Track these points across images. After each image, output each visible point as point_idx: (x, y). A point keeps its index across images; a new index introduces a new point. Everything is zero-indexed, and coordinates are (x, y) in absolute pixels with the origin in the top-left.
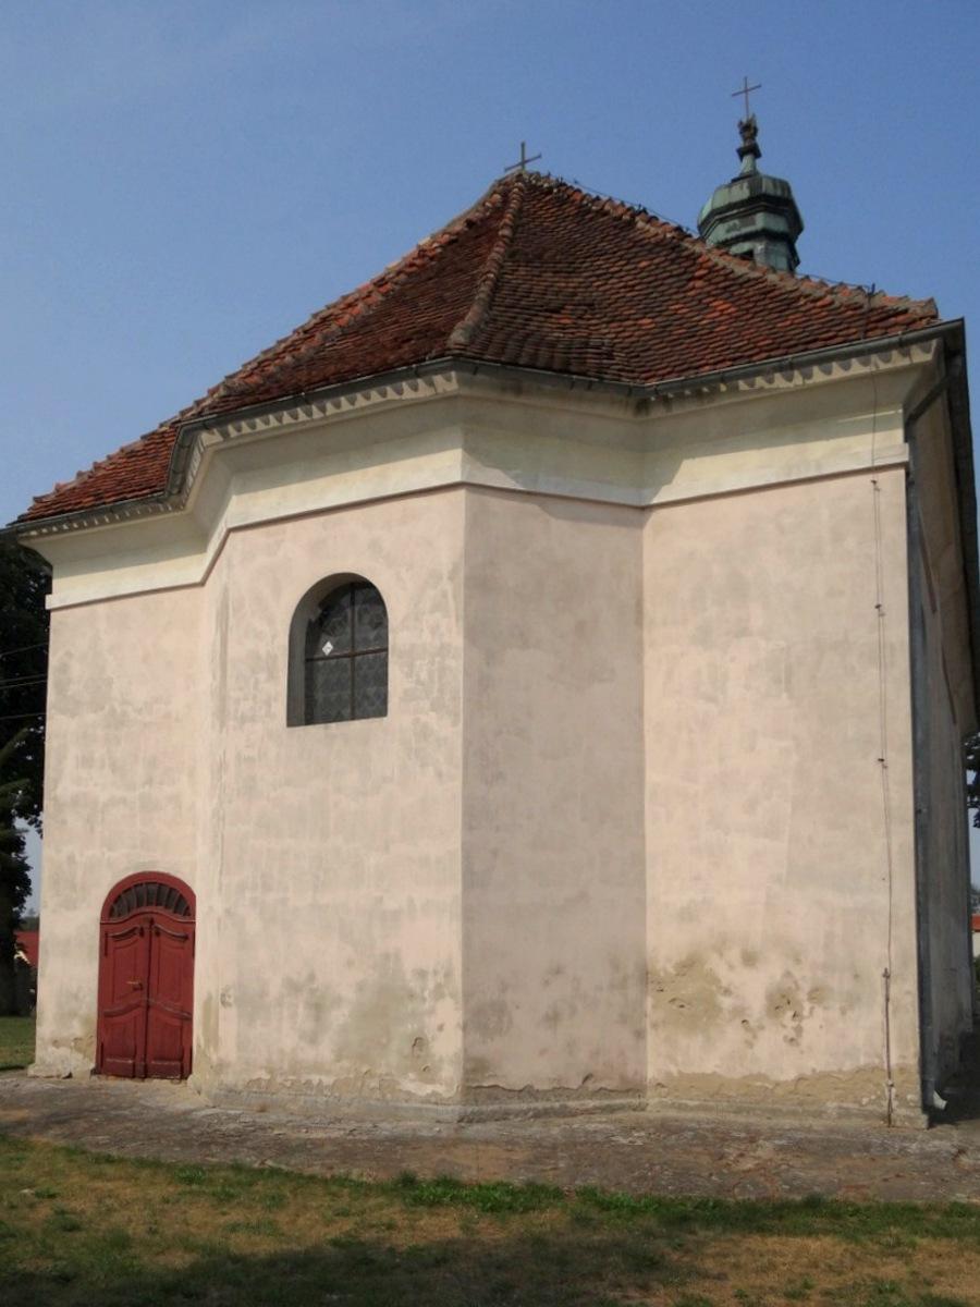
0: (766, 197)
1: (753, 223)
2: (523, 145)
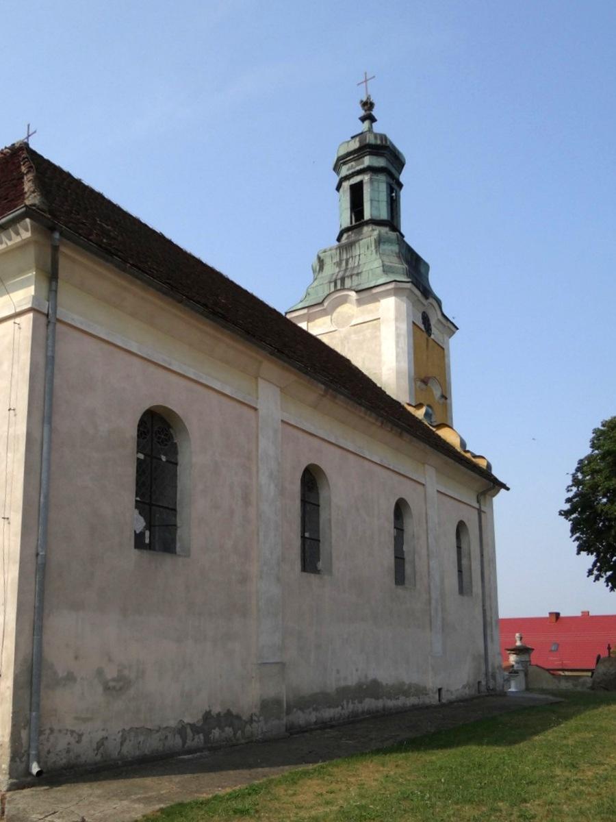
0: (369, 146)
1: (363, 163)
2: (29, 126)
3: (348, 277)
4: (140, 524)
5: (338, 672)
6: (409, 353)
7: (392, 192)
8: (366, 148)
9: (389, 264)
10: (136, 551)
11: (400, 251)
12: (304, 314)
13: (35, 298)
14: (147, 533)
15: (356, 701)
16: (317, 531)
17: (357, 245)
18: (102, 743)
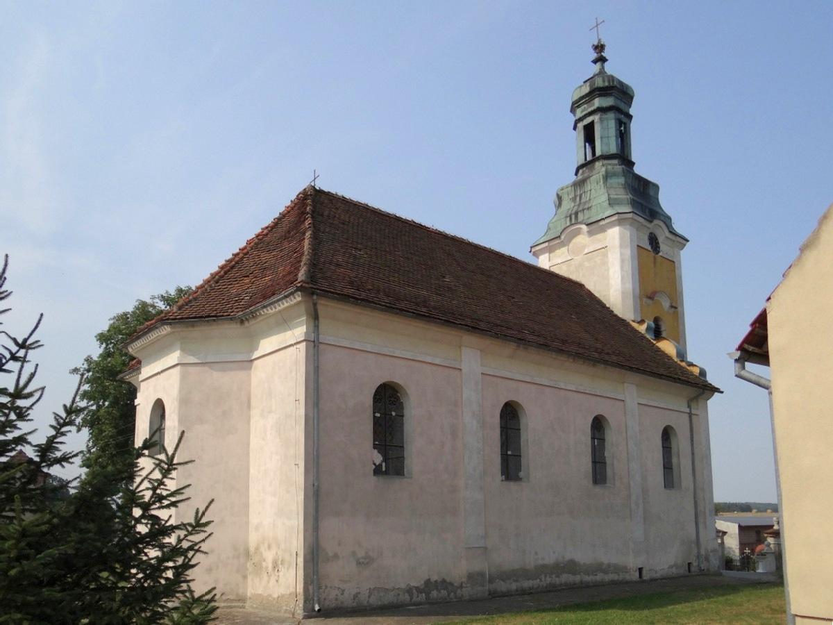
1: (594, 105)
2: (315, 171)
3: (580, 211)
4: (378, 458)
5: (536, 553)
6: (633, 275)
7: (621, 127)
8: (595, 92)
9: (616, 197)
10: (375, 478)
11: (626, 182)
12: (547, 247)
13: (306, 333)
14: (384, 464)
15: (554, 576)
16: (519, 449)
17: (588, 181)
18: (356, 596)
